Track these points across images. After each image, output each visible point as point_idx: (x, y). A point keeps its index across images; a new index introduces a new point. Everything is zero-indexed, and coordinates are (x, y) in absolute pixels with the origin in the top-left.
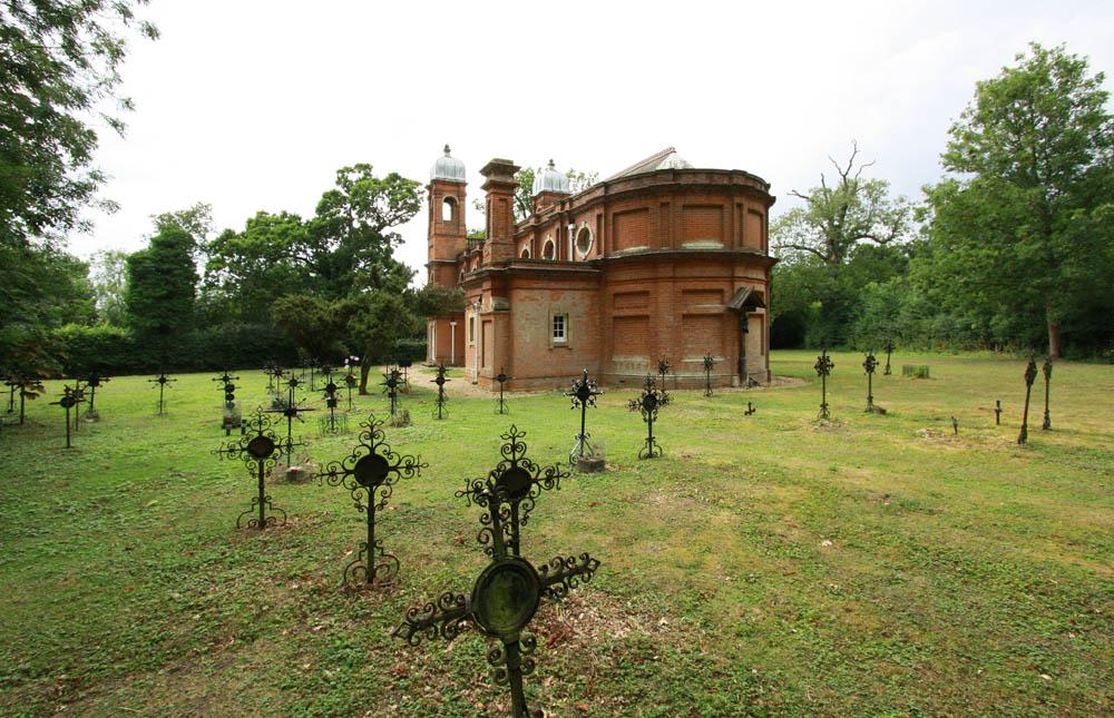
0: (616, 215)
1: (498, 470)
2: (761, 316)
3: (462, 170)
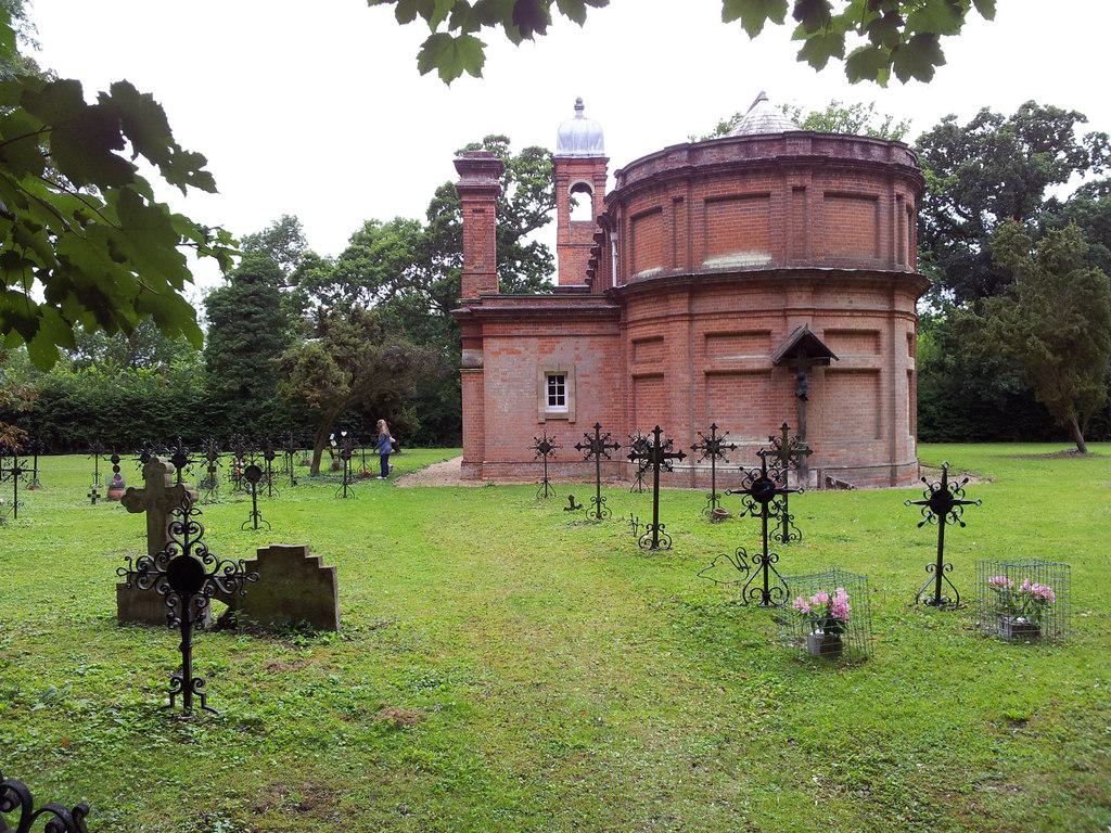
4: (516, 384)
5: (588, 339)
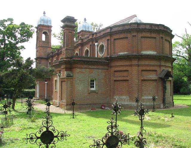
0: (115, 39)
1: (106, 136)
2: (170, 81)
3: (50, 21)
4: (83, 82)
5: (101, 70)
